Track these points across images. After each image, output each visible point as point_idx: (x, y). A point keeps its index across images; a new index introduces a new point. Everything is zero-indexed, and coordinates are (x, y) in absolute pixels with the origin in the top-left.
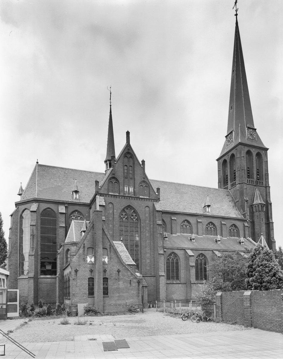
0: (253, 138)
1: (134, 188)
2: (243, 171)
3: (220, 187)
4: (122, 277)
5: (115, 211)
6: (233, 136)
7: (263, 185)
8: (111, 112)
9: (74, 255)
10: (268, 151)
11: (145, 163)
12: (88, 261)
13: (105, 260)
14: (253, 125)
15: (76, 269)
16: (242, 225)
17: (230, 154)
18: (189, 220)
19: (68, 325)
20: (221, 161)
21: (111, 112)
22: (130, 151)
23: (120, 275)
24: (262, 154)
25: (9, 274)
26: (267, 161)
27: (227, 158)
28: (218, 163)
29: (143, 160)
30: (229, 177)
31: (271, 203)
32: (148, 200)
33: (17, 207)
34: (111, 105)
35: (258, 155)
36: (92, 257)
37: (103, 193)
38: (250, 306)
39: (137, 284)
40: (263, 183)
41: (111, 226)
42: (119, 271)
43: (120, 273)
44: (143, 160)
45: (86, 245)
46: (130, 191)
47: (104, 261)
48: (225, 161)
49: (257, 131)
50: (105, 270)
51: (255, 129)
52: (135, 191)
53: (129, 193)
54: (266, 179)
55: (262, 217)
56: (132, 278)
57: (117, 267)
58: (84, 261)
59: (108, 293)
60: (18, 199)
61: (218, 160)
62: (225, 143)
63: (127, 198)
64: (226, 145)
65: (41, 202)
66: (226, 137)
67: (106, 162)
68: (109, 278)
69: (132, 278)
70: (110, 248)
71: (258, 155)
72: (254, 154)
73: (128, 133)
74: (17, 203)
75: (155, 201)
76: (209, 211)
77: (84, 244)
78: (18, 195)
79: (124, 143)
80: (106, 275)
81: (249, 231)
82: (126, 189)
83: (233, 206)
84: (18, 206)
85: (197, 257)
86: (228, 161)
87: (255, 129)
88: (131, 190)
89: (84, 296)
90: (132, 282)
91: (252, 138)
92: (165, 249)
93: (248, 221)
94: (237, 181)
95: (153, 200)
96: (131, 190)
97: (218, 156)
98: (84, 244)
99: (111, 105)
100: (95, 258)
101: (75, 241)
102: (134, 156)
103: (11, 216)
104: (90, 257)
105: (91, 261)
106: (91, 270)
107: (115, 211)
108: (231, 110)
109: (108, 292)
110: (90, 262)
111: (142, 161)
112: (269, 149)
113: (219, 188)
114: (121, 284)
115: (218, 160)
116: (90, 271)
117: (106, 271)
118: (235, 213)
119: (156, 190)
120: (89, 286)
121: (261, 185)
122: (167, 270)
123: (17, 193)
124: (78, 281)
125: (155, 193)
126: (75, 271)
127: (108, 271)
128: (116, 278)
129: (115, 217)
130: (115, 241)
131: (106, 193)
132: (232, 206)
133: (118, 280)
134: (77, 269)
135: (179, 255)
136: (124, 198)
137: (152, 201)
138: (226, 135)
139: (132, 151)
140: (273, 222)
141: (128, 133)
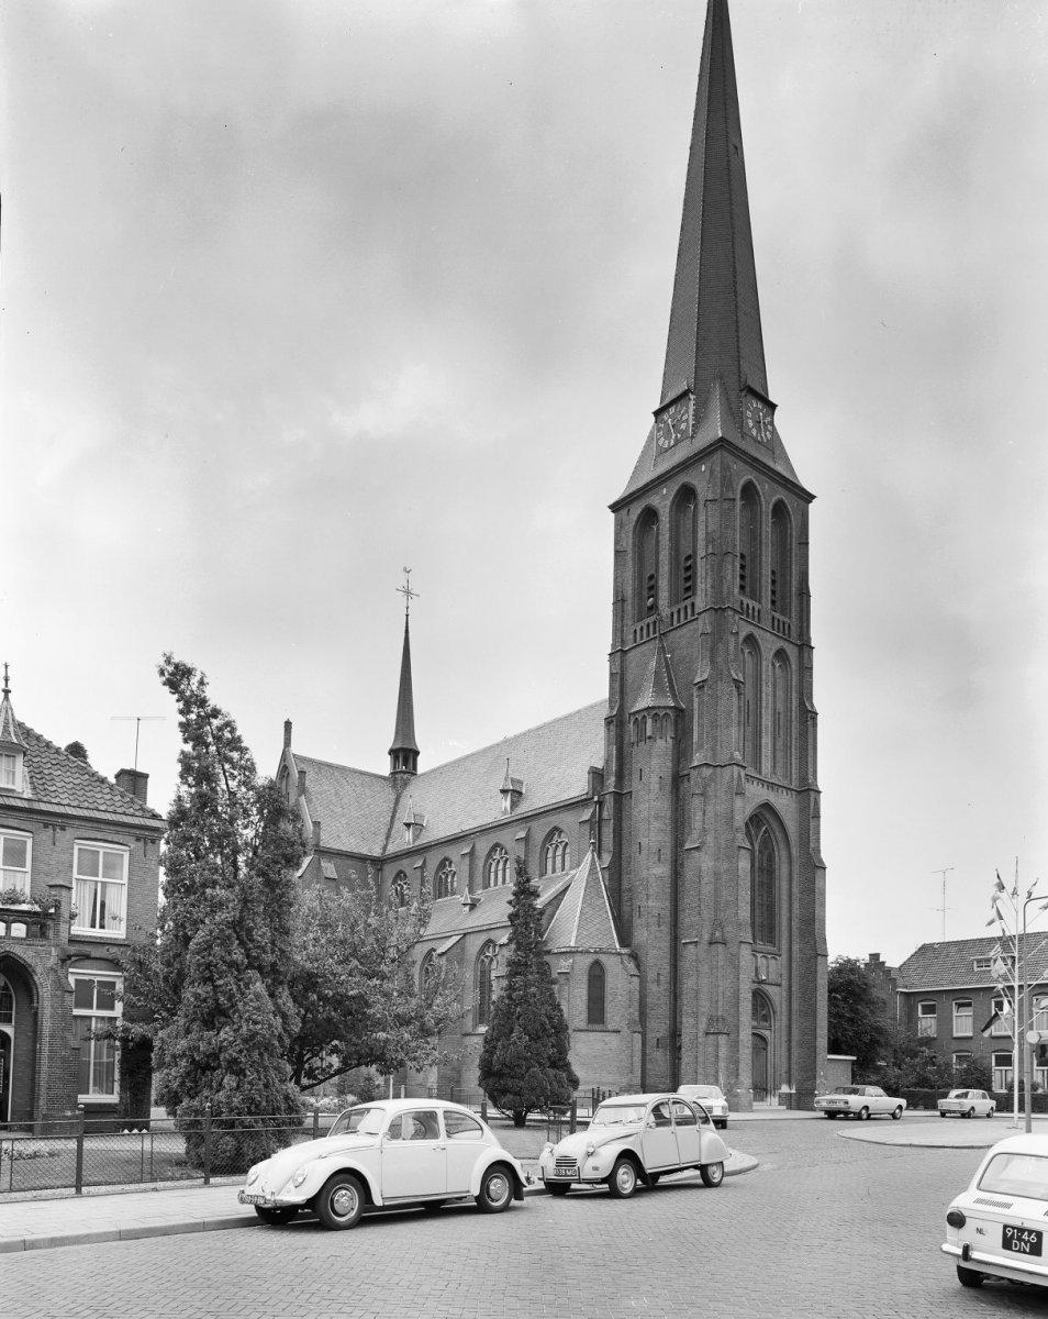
2: (730, 558)
6: (687, 412)
8: (407, 631)
10: (811, 505)
20: (636, 510)
21: (407, 631)
26: (807, 543)
27: (663, 501)
28: (616, 519)
34: (407, 615)
35: (779, 510)
38: (692, 437)
48: (650, 515)
51: (773, 407)
61: (615, 507)
64: (653, 450)
66: (657, 414)
67: (392, 752)
71: (779, 510)
72: (767, 508)
87: (773, 407)
94: (701, 601)
97: (618, 493)
99: (407, 615)
101: (572, 944)
115: (615, 507)
138: (657, 406)
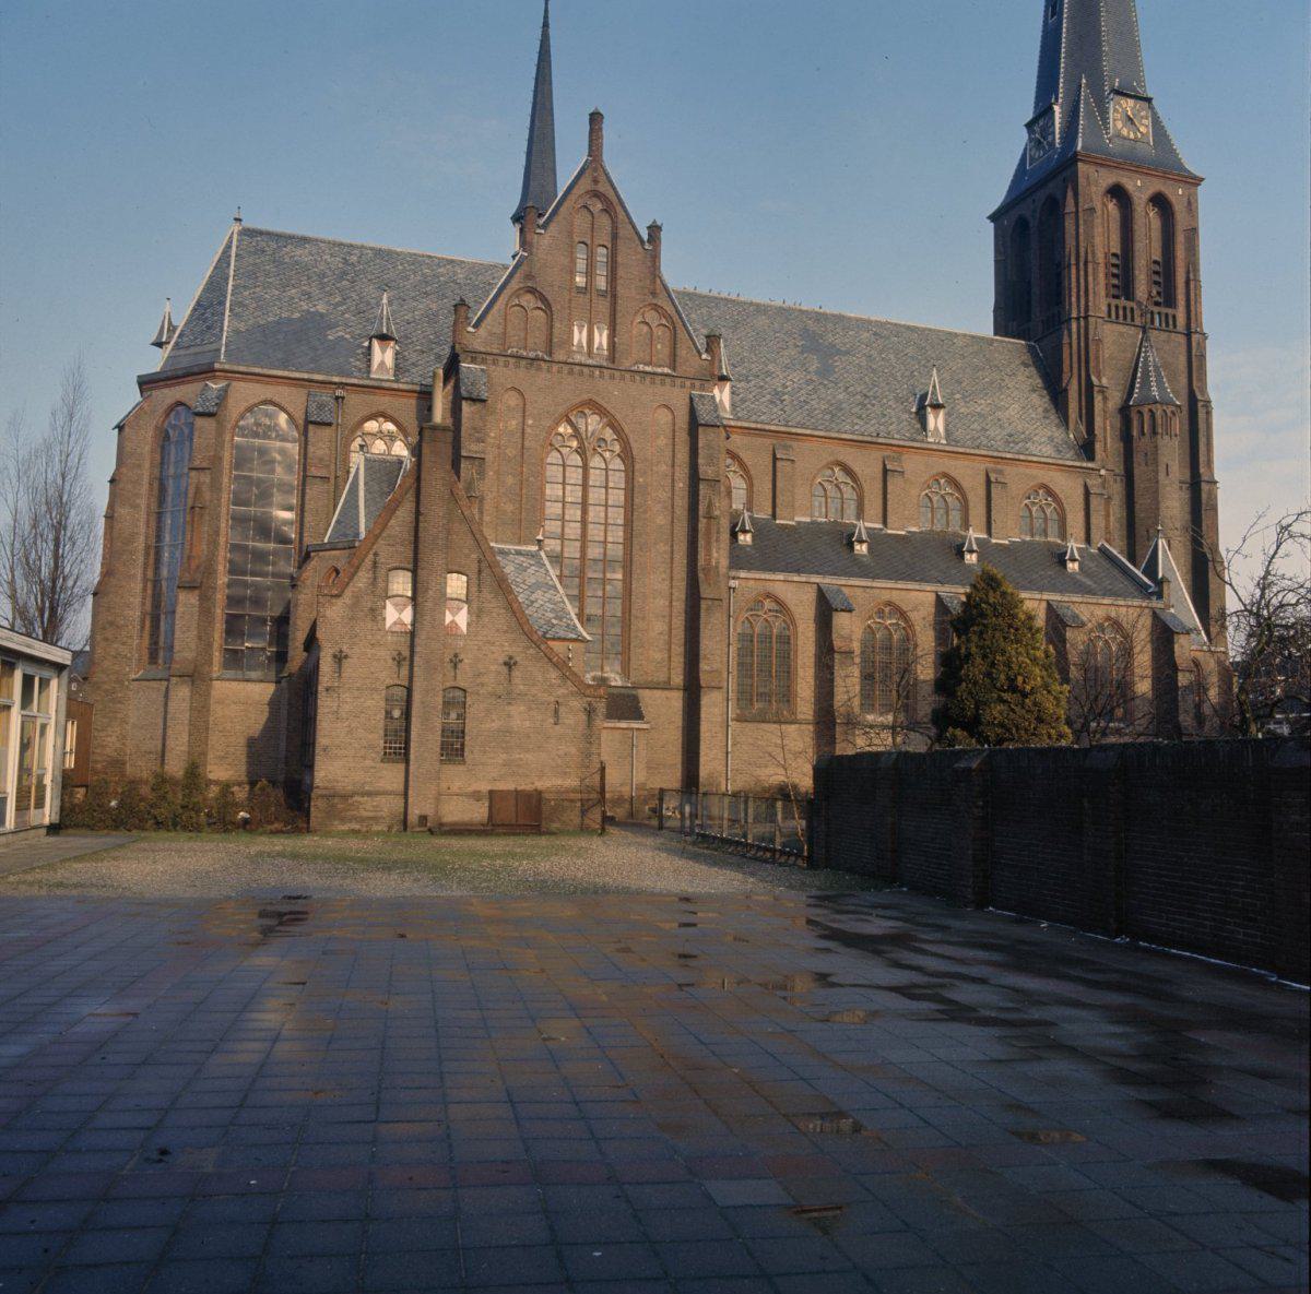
0: (1135, 133)
1: (614, 330)
3: (1000, 328)
4: (522, 687)
5: (530, 422)
7: (1175, 326)
8: (546, 25)
9: (332, 596)
11: (663, 235)
12: (389, 623)
13: (457, 619)
14: (1140, 81)
15: (341, 651)
16: (1081, 491)
17: (1041, 195)
18: (851, 464)
19: (680, 950)
21: (546, 25)
22: (603, 188)
23: (516, 681)
24: (1173, 199)
25: (69, 663)
29: (655, 221)
30: (1035, 290)
31: (1209, 402)
32: (668, 380)
33: (146, 394)
36: (405, 606)
37: (483, 350)
39: (584, 717)
40: (1174, 317)
41: (510, 480)
42: (510, 664)
43: (516, 673)
44: (655, 221)
45: (381, 559)
46: (596, 346)
47: (453, 622)
48: (1022, 224)
49: (1154, 102)
50: (456, 656)
52: (614, 343)
53: (590, 353)
54: (1196, 295)
55: (1163, 460)
56: (562, 691)
57: (505, 646)
58: (374, 619)
59: (462, 749)
60: (155, 362)
61: (994, 218)
62: (1025, 149)
63: (592, 376)
65: (238, 380)
66: (1029, 126)
68: (469, 690)
69: (562, 691)
70: (480, 572)
73: (595, 119)
74: (145, 379)
75: (697, 383)
76: (936, 428)
77: (376, 554)
78: (153, 344)
79: (582, 158)
80: (459, 677)
81: (1108, 515)
82: (579, 336)
83: (1046, 411)
84: (151, 389)
85: (870, 618)
86: (1033, 223)
88: (601, 338)
89: (364, 758)
90: (562, 710)
91: (1132, 136)
92: (734, 578)
93: (1103, 472)
95: (688, 383)
96: (601, 340)
98: (376, 554)
100: (415, 607)
102: (619, 208)
103: (120, 428)
104: (396, 605)
105: (399, 622)
106: (400, 654)
107: (530, 422)
108: (1052, 17)
109: (463, 745)
110: (395, 623)
111: (649, 228)
112: (1202, 179)
113: (995, 334)
114: (519, 717)
115: (994, 218)
116: (394, 659)
117: (461, 661)
118: (1051, 439)
119: (701, 342)
120: (386, 718)
121: (1167, 325)
122: (739, 664)
123: (153, 338)
124: (346, 696)
125: (699, 352)
126: (335, 656)
127: (466, 661)
128: (500, 690)
129: (527, 444)
130: (946, 420)
131: (495, 351)
132: (1040, 410)
133: (509, 697)
134: (345, 648)
135: (792, 608)
136: (571, 372)
137: (683, 386)
139: (609, 187)
140: (1216, 478)
141: (595, 119)
